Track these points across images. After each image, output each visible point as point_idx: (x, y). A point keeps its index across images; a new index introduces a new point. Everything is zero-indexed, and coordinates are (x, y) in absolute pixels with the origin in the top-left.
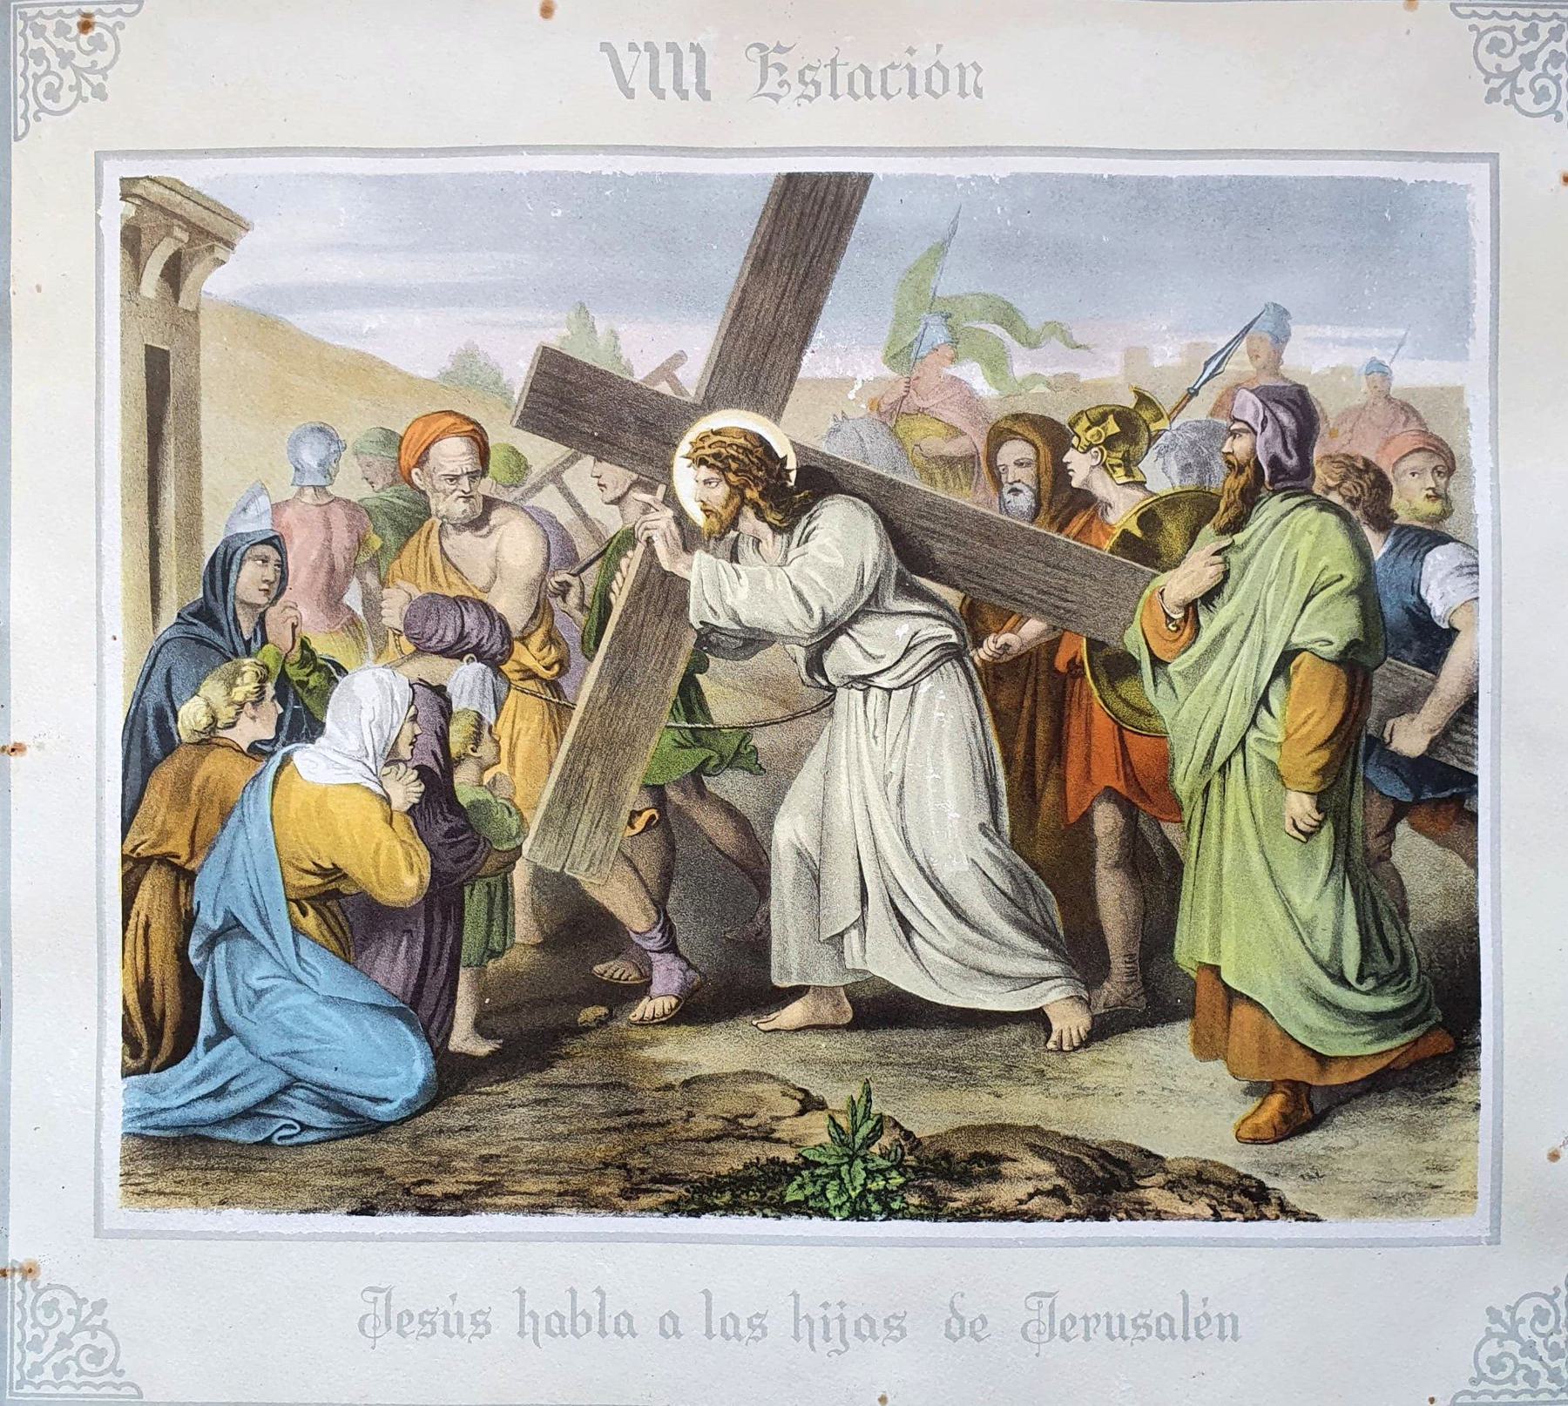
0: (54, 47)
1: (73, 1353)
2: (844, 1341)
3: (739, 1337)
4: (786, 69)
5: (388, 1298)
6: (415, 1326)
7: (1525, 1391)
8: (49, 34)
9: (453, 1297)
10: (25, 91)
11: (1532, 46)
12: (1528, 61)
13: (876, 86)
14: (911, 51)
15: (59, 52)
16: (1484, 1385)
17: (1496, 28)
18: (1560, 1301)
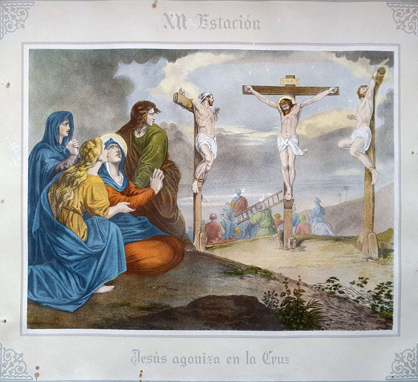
0: (10, 14)
1: (14, 368)
2: (185, 364)
3: (283, 363)
4: (207, 21)
5: (139, 352)
6: (146, 360)
7: (405, 376)
8: (9, 11)
9: (156, 353)
10: (3, 26)
11: (409, 14)
12: (407, 18)
13: (231, 26)
14: (241, 16)
15: (12, 16)
16: (3, 351)
17: (400, 10)
18: (415, 352)
